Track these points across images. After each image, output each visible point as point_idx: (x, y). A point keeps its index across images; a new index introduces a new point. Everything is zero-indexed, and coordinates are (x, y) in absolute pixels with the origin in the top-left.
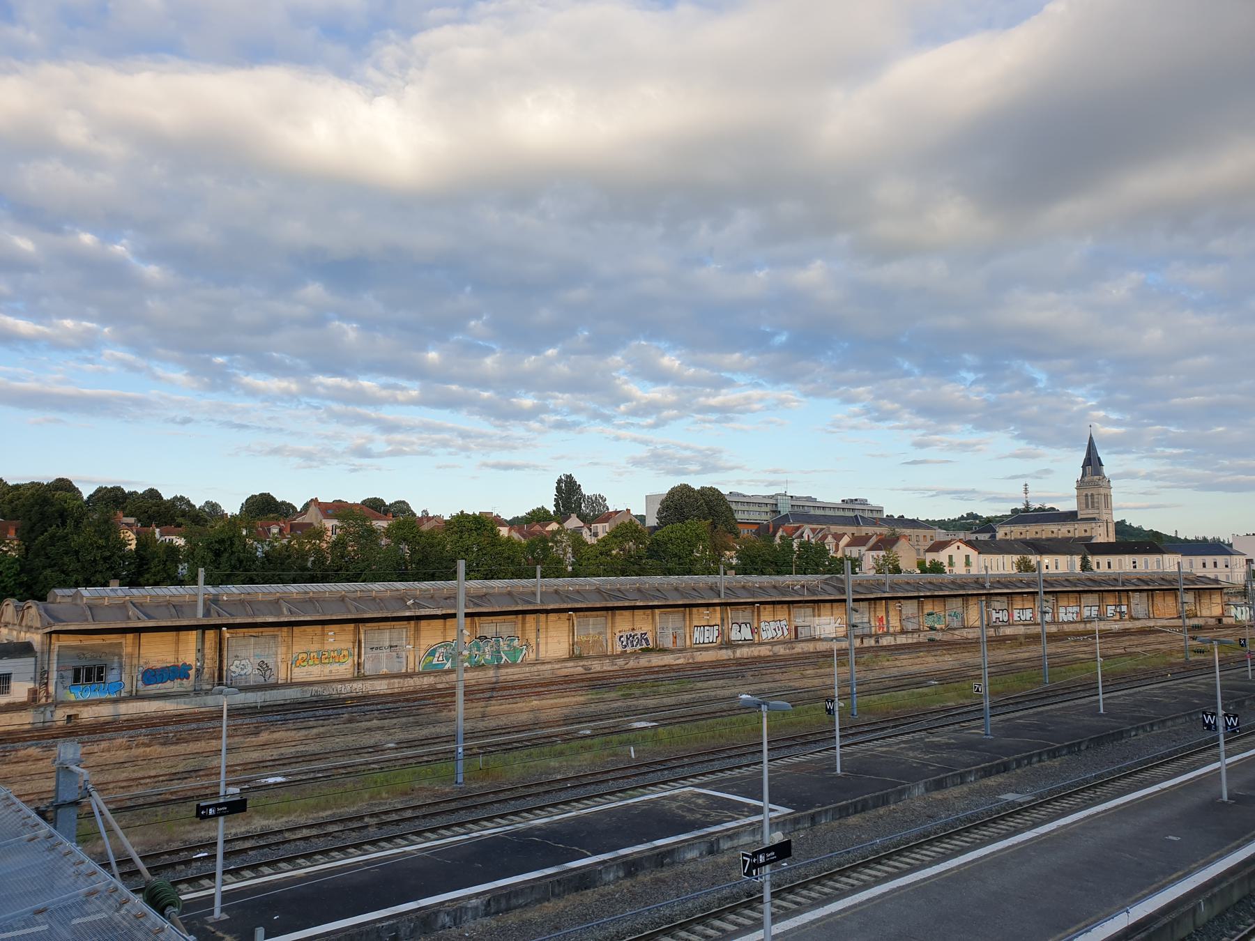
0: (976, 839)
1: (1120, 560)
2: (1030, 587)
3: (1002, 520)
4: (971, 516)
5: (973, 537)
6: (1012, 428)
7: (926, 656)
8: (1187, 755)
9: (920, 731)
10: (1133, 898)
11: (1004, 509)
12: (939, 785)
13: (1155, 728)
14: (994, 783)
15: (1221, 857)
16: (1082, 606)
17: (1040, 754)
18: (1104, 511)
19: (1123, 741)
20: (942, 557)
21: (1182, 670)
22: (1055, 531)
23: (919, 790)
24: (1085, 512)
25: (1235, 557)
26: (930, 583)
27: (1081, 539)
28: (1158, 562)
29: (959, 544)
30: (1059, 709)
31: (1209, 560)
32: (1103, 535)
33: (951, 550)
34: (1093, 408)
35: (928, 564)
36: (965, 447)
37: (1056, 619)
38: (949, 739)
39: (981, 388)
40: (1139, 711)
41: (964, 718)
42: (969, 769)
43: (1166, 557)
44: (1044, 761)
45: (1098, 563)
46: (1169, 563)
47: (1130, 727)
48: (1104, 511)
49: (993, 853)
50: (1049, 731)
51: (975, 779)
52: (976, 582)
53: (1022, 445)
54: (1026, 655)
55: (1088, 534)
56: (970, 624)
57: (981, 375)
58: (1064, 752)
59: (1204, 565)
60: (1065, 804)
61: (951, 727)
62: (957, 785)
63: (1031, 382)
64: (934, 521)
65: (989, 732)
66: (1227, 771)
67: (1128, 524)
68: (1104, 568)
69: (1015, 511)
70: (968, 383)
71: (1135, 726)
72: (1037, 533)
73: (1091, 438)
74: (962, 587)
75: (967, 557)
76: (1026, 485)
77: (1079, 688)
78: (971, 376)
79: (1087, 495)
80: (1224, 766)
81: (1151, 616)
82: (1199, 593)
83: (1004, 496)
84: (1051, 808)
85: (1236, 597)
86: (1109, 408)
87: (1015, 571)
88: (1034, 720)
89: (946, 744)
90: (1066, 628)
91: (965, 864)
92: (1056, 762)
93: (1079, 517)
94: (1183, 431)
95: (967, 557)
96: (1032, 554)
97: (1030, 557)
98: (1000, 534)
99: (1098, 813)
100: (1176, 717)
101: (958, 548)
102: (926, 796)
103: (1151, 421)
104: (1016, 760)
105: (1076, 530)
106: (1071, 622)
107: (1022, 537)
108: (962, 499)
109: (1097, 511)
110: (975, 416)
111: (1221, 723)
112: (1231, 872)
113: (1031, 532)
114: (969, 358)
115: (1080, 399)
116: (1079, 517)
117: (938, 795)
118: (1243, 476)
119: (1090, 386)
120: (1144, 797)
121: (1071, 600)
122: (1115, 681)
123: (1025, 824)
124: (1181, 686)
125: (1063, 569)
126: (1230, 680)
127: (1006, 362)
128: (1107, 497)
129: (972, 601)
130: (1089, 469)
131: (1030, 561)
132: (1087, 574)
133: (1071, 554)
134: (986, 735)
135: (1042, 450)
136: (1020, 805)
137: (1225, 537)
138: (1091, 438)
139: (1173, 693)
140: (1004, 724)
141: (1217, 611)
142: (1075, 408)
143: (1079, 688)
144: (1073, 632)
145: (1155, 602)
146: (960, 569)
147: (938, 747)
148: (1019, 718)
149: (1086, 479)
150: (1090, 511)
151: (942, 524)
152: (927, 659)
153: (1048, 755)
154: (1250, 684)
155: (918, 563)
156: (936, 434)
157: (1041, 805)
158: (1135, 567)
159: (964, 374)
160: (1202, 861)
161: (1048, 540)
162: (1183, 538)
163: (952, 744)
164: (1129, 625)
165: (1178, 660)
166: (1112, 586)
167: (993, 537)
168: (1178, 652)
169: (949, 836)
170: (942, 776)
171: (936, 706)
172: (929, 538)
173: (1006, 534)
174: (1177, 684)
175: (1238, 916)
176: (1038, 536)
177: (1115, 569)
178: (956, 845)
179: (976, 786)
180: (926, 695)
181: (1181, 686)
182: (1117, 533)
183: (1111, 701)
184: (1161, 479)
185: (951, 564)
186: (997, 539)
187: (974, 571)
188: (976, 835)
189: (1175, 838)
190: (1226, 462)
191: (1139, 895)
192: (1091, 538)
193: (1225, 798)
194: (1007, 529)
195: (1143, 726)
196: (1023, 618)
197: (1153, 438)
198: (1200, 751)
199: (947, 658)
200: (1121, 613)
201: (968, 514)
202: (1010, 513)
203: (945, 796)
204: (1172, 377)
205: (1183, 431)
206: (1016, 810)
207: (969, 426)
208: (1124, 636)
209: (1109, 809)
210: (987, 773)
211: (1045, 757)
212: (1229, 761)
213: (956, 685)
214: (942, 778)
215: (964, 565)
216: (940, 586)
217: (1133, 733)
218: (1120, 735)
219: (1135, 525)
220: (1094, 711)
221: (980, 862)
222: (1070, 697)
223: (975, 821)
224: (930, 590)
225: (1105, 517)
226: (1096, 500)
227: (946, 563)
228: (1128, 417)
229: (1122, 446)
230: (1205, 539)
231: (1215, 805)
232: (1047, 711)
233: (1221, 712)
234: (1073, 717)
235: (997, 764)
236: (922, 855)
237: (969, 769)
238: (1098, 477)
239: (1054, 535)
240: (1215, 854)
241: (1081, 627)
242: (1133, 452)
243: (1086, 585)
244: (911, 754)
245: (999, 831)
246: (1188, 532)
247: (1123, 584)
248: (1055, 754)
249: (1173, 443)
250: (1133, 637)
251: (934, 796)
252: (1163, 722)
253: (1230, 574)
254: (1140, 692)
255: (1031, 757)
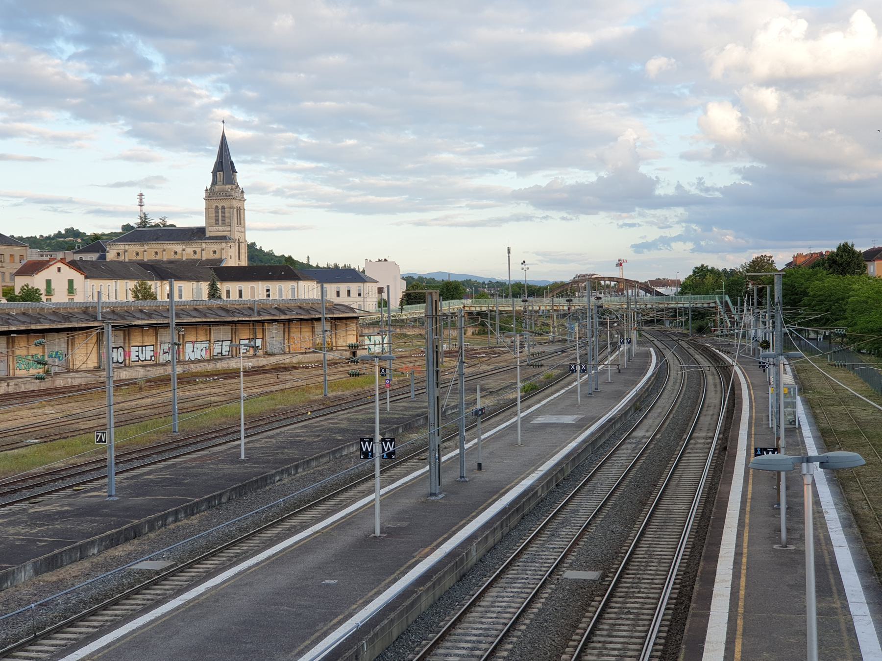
0: (107, 621)
1: (253, 288)
2: (151, 318)
3: (114, 238)
4: (72, 233)
5: (77, 257)
6: (122, 122)
7: (21, 410)
8: (334, 495)
9: (20, 501)
10: (296, 651)
11: (112, 225)
12: (53, 564)
13: (299, 471)
14: (123, 554)
15: (378, 593)
16: (212, 341)
17: (176, 512)
18: (236, 229)
19: (267, 488)
20: (37, 281)
21: (322, 407)
22: (179, 251)
23: (25, 574)
24: (214, 229)
25: (368, 284)
26: (24, 314)
27: (209, 262)
28: (293, 290)
29: (60, 265)
30: (195, 459)
31: (343, 287)
32: (234, 258)
33: (49, 273)
34: (217, 105)
35: (17, 292)
36: (61, 140)
37: (182, 358)
38: (62, 506)
39: (82, 65)
40: (282, 453)
41: (78, 480)
42: (91, 539)
43: (301, 283)
44: (180, 521)
45: (228, 292)
46: (308, 291)
47: (274, 471)
48: (236, 229)
49: (133, 632)
50: (185, 484)
51: (99, 551)
52: (85, 312)
53: (133, 145)
54: (148, 401)
55: (217, 256)
56: (76, 367)
57: (82, 49)
58: (203, 508)
59: (338, 294)
60: (209, 564)
61: (62, 493)
62: (76, 561)
63: (144, 64)
64: (21, 238)
65: (114, 493)
66: (522, 421)
67: (258, 247)
68: (234, 296)
69: (126, 228)
70: (65, 57)
71: (280, 470)
72: (156, 253)
73: (223, 137)
74: (67, 319)
75: (71, 282)
76: (141, 195)
77: (214, 435)
78: (70, 49)
79: (217, 208)
80: (378, 497)
81: (287, 350)
82: (336, 322)
83: (111, 209)
84: (239, 549)
85: (368, 328)
86: (235, 107)
87: (131, 298)
88: (167, 475)
89: (59, 512)
90: (194, 368)
91: (98, 651)
92: (195, 520)
93: (207, 235)
94: (314, 141)
95: (71, 282)
96: (151, 279)
97: (149, 283)
98: (111, 256)
99: (250, 568)
100: (321, 456)
101: (59, 270)
102: (34, 579)
103: (282, 127)
104: (148, 521)
105: (204, 251)
106: (199, 361)
107: (139, 258)
108: (55, 210)
109: (228, 228)
110: (75, 101)
111: (377, 450)
112: (389, 607)
113: (149, 252)
114: (67, 23)
115: (204, 92)
116: (207, 235)
117: (50, 577)
118: (373, 197)
119: (214, 77)
120: (296, 543)
121: (199, 331)
122: (256, 423)
123: (165, 594)
124: (323, 423)
125: (187, 297)
126: (370, 413)
127: (115, 35)
128: (240, 211)
129: (80, 338)
130: (220, 175)
131: (150, 288)
132: (215, 303)
133: (198, 279)
134: (110, 496)
135: (158, 152)
136: (157, 573)
137: (358, 265)
138: (223, 137)
139: (317, 431)
140: (129, 482)
141: (352, 340)
142: (197, 103)
143: (214, 435)
144: (201, 373)
145: (291, 335)
146: (60, 297)
147: (49, 517)
148: (149, 473)
149: (217, 188)
150: (220, 228)
151: (33, 242)
152: (21, 413)
153: (186, 512)
154: (388, 416)
155: (3, 290)
156: (21, 120)
157: (182, 570)
158: (268, 296)
159: (60, 43)
160: (361, 601)
161: (171, 262)
162: (315, 266)
163: (67, 511)
164: (262, 361)
165: (316, 397)
166: (247, 316)
167: (103, 257)
168: (317, 388)
169: (71, 624)
170: (56, 551)
171: (39, 469)
172: (17, 258)
173: (118, 254)
174: (318, 422)
175: (398, 653)
176: (158, 257)
177: (246, 297)
178: (80, 633)
179: (100, 559)
180: (24, 456)
181: (323, 423)
182: (250, 258)
183: (251, 445)
184: (293, 196)
185: (49, 291)
186: (108, 260)
187: (79, 298)
188: (108, 615)
189: (332, 582)
190: (357, 180)
191: (302, 647)
192: (221, 261)
193: (378, 533)
194: (120, 248)
195: (288, 469)
196: (142, 357)
197: (283, 147)
198: (346, 490)
199: (48, 410)
200: (255, 348)
201: (67, 230)
202: (120, 231)
203: (61, 577)
204: (302, 75)
205: (314, 141)
206: (155, 579)
207: (67, 115)
208: (258, 374)
209: (262, 562)
210: (114, 541)
211: (182, 515)
212: (383, 491)
213: (63, 441)
214: (56, 555)
215: (66, 292)
216: (37, 319)
217: (277, 478)
218: (264, 480)
219: (266, 249)
220: (235, 458)
221: (118, 645)
222: (205, 444)
223: (102, 600)
224: (23, 323)
225: (237, 236)
226: (227, 215)
227: (42, 288)
228: (255, 119)
229: (255, 149)
230: (336, 266)
231: (368, 542)
232: (180, 463)
233: (378, 438)
234: (211, 466)
235: (126, 529)
236: (38, 652)
237: (91, 539)
238: (230, 186)
239: (177, 257)
240: (373, 592)
241: (210, 367)
242: (262, 163)
243: (217, 315)
244: (11, 530)
245: (134, 607)
246: (320, 260)
247: (259, 315)
248: (193, 511)
249: (304, 154)
250: (267, 375)
251: (46, 579)
252: (308, 462)
253: (362, 303)
254: (281, 433)
255: (164, 518)
